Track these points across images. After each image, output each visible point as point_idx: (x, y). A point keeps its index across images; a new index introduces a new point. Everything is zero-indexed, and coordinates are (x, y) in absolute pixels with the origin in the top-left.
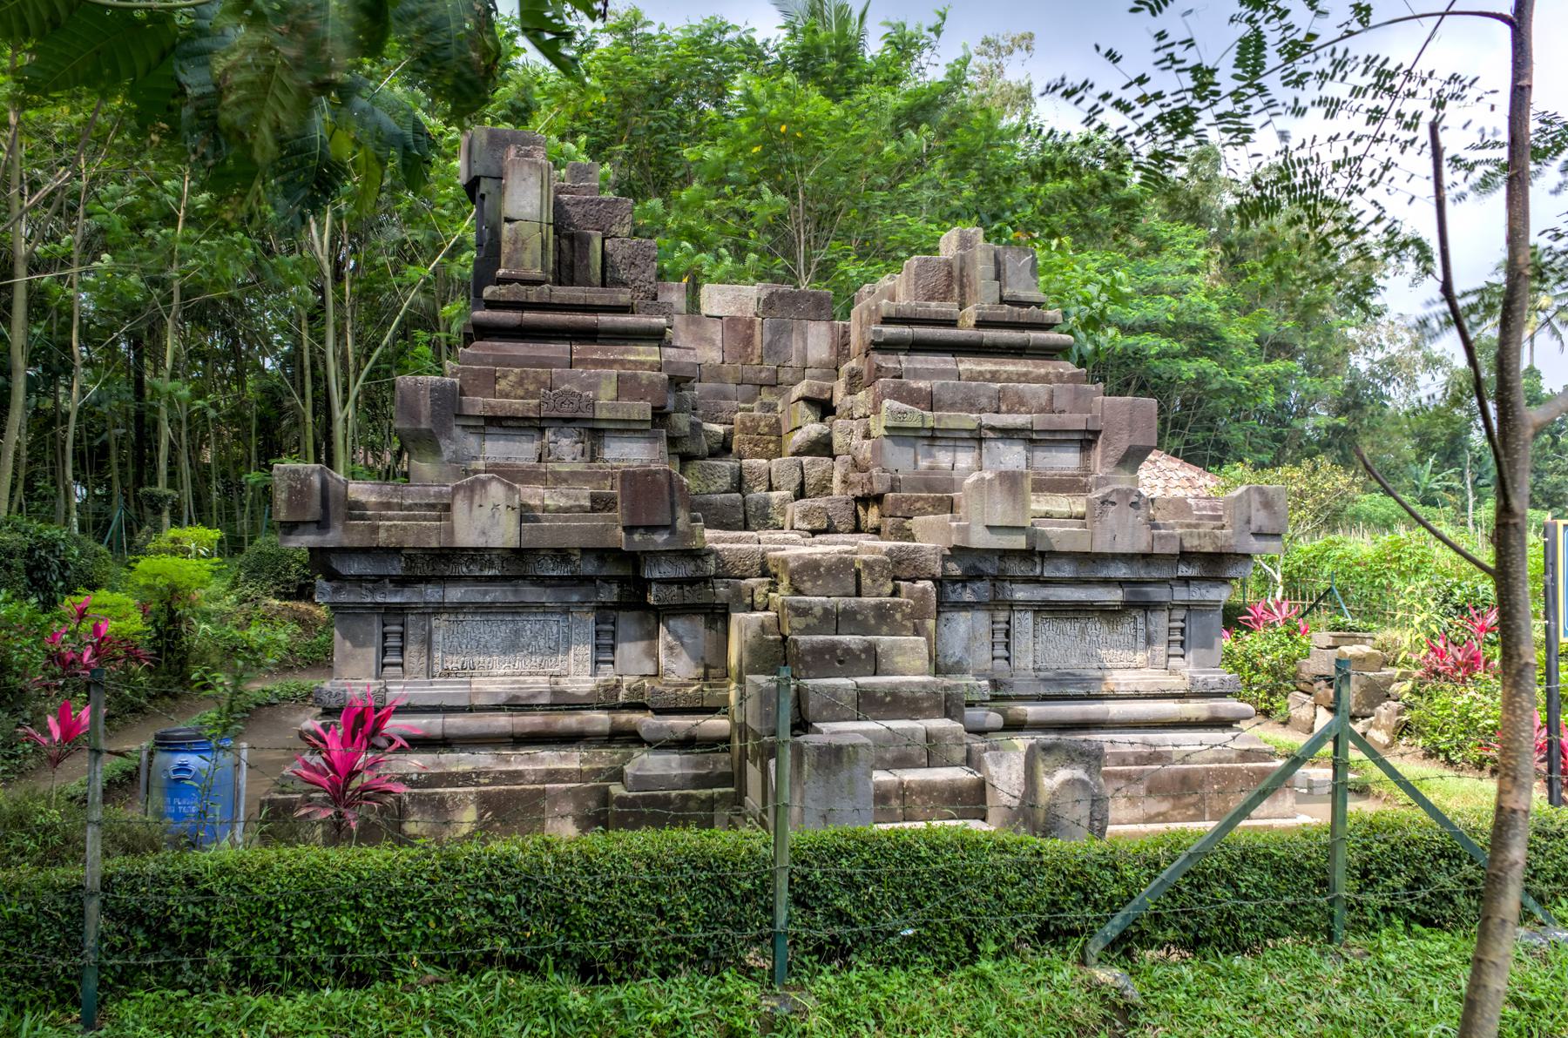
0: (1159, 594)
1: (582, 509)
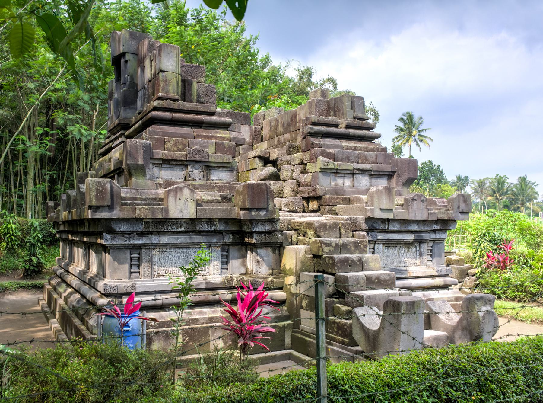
0: (426, 236)
1: (218, 201)
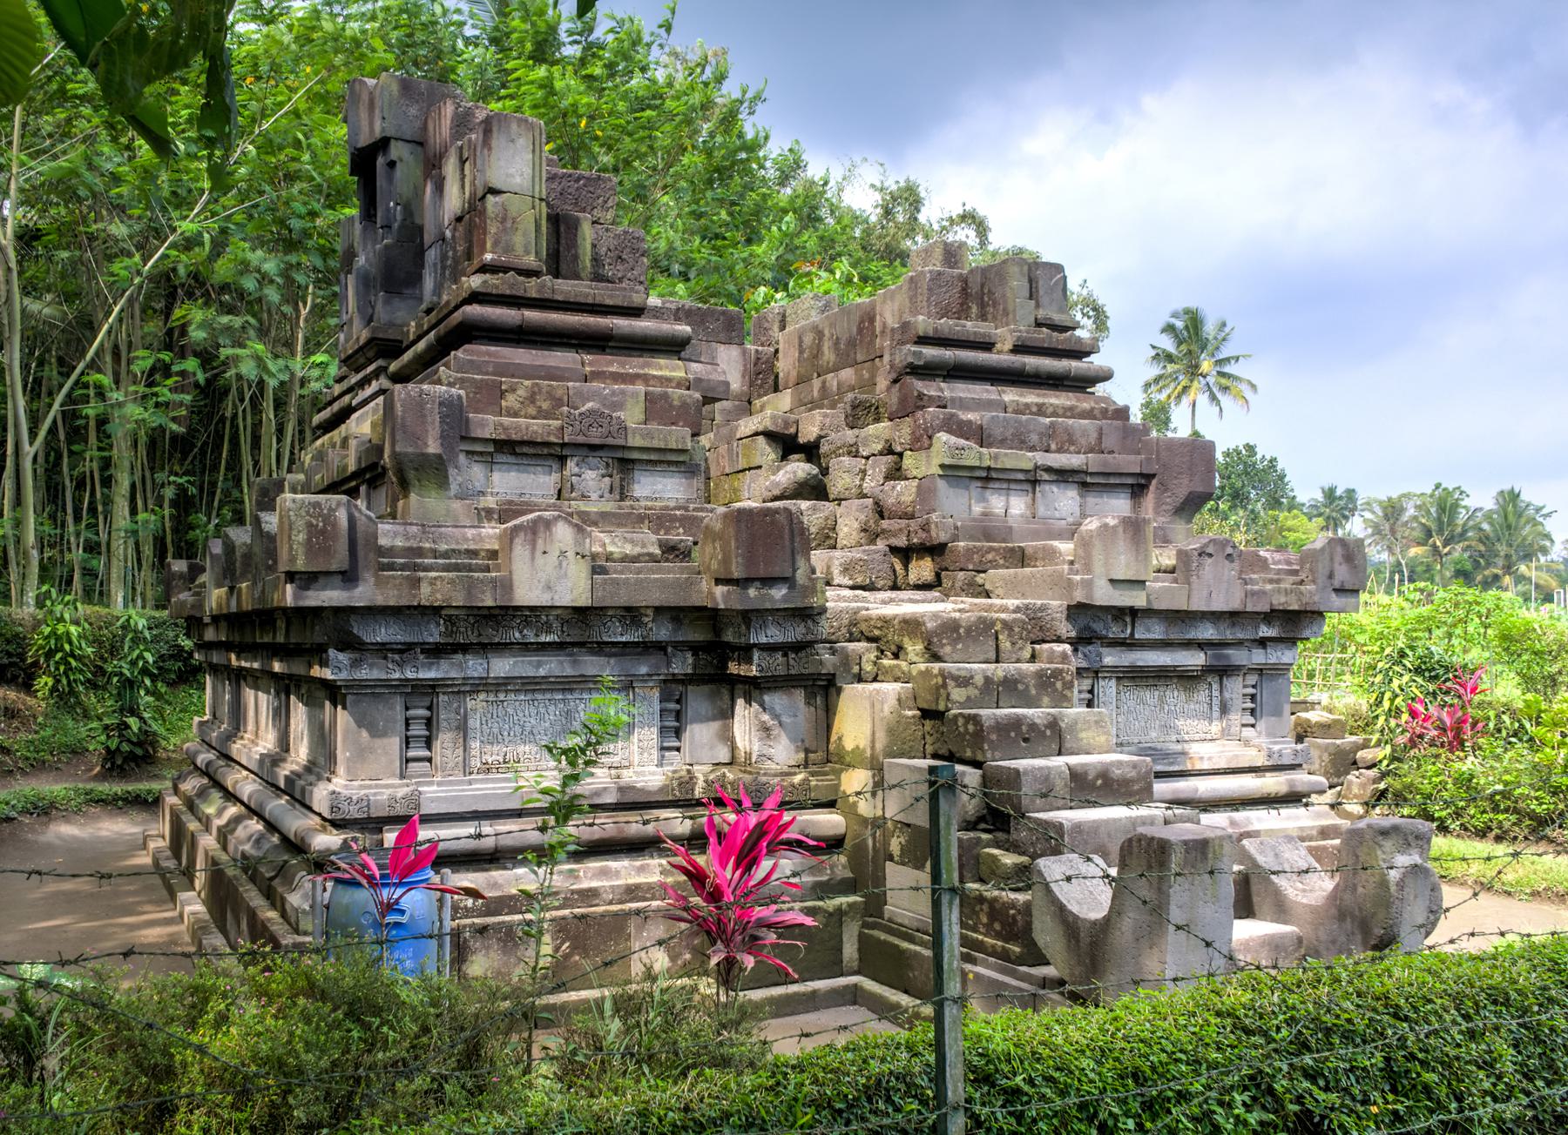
0: (1238, 656)
1: (652, 558)
